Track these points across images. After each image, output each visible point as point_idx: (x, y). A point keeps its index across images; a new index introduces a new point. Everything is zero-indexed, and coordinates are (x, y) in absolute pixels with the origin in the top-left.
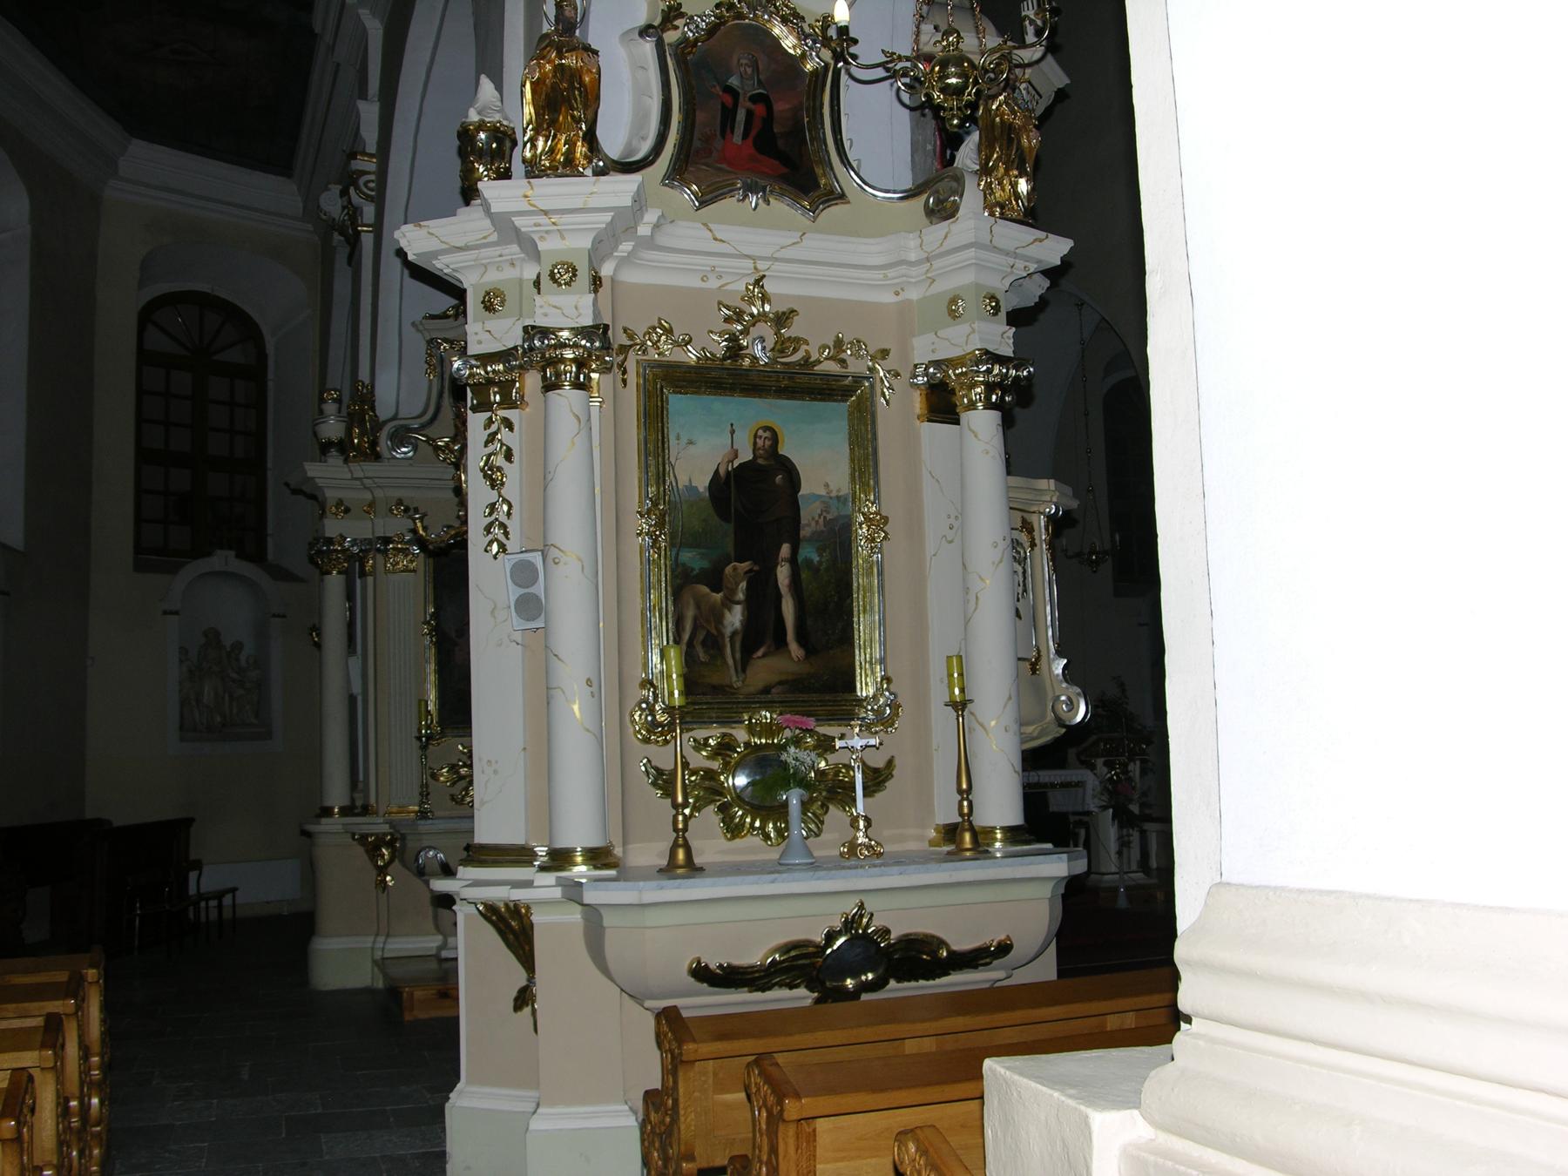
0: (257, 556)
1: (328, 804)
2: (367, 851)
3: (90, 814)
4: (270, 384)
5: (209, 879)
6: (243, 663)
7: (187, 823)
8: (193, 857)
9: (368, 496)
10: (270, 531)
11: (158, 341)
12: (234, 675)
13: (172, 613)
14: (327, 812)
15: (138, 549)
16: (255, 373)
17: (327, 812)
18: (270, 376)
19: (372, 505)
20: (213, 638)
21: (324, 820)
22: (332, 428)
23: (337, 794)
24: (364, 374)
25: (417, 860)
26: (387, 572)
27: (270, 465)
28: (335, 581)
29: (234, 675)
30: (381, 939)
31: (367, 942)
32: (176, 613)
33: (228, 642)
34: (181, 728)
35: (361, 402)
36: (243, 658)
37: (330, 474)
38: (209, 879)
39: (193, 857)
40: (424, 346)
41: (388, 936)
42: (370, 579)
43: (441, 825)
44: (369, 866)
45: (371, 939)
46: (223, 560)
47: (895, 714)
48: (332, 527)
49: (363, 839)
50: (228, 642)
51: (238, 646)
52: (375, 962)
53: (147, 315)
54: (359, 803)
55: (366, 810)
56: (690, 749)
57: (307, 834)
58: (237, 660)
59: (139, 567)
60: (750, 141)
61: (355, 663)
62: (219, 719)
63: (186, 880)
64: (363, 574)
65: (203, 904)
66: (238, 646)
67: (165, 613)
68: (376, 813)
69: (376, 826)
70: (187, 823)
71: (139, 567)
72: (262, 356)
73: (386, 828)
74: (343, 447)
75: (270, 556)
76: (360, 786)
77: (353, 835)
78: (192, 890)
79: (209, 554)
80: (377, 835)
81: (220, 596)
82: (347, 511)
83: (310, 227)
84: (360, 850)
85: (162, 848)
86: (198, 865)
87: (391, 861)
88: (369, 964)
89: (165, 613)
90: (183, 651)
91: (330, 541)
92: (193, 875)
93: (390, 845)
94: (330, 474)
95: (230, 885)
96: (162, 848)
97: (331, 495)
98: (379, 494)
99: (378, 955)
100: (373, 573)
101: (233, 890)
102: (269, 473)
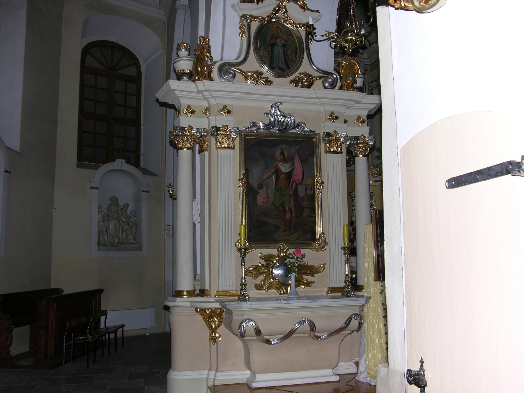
0: (136, 164)
1: (180, 288)
2: (204, 318)
3: (53, 286)
4: (143, 86)
5: (111, 320)
6: (129, 214)
7: (100, 291)
8: (102, 309)
9: (205, 104)
10: (142, 153)
11: (91, 62)
12: (124, 220)
13: (94, 188)
14: (179, 294)
15: (80, 157)
16: (137, 80)
17: (179, 294)
18: (143, 81)
19: (208, 109)
20: (114, 201)
21: (178, 299)
22: (185, 64)
23: (185, 283)
24: (201, 32)
25: (240, 327)
26: (217, 148)
27: (142, 123)
28: (185, 154)
29: (124, 220)
30: (213, 373)
31: (203, 374)
32: (97, 188)
33: (121, 204)
34: (99, 244)
35: (201, 53)
36: (128, 211)
37: (182, 91)
38: (111, 320)
39: (102, 309)
40: (238, 19)
41: (217, 371)
42: (206, 153)
43: (256, 305)
44: (206, 327)
45: (206, 372)
46: (120, 164)
47: (325, 245)
48: (184, 121)
49: (202, 311)
50: (121, 204)
51: (126, 206)
52: (209, 388)
53: (87, 51)
54: (198, 288)
55: (202, 293)
56: (256, 256)
57: (167, 308)
58: (126, 212)
59: (79, 166)
60: (276, 80)
61: (197, 204)
62: (117, 240)
63: (99, 320)
64: (201, 151)
65: (107, 335)
66: (126, 206)
67: (92, 188)
68: (209, 295)
69: (211, 303)
70: (100, 291)
71: (79, 166)
72: (139, 73)
73: (217, 305)
74: (191, 76)
75: (142, 165)
76: (198, 277)
77: (196, 308)
78: (102, 326)
79: (114, 161)
80: (211, 309)
81: (117, 180)
82: (193, 112)
83: (162, 12)
84: (200, 317)
85: (88, 304)
86: (105, 313)
87: (218, 326)
88: (205, 388)
89: (92, 188)
90: (100, 207)
91: (183, 129)
92: (103, 318)
93: (220, 315)
94: (182, 91)
95: (121, 323)
96: (88, 304)
97: (184, 102)
98: (213, 102)
99: (211, 384)
100: (209, 150)
101: (123, 326)
102: (142, 126)
